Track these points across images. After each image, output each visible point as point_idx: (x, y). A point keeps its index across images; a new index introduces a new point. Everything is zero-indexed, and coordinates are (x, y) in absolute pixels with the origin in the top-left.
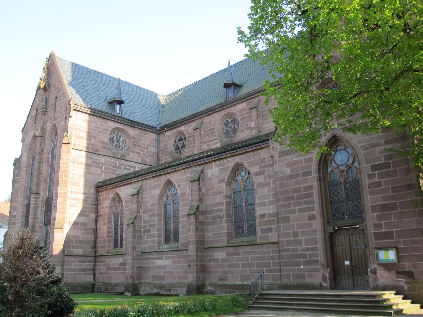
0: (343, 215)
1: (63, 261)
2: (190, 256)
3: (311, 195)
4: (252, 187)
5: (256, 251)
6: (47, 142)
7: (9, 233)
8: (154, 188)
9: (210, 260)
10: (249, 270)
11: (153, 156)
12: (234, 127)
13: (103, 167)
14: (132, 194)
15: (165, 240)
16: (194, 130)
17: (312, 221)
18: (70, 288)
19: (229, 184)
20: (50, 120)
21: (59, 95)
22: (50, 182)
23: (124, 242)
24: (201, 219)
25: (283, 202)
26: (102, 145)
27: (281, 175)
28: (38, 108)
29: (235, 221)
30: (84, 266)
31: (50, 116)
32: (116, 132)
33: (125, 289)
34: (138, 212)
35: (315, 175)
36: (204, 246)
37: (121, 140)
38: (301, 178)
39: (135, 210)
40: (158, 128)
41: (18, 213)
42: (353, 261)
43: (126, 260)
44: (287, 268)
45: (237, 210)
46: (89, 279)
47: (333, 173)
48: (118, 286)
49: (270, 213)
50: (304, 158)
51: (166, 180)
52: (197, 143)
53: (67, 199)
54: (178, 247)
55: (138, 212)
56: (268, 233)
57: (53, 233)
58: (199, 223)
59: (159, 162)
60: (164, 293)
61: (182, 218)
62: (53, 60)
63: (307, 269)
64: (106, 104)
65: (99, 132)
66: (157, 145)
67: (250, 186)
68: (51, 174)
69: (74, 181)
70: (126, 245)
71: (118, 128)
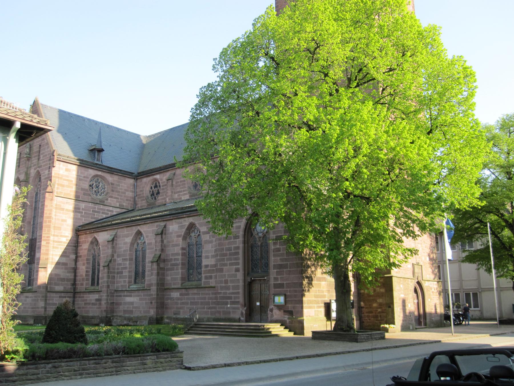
2: (152, 295)
5: (200, 292)
8: (127, 236)
9: (168, 299)
11: (130, 200)
16: (167, 180)
17: (237, 273)
19: (184, 238)
20: (33, 166)
21: (43, 144)
22: (34, 224)
23: (100, 281)
24: (162, 265)
25: (220, 257)
26: (83, 192)
28: (22, 153)
31: (34, 163)
32: (96, 179)
34: (113, 256)
35: (241, 239)
36: (163, 287)
37: (100, 186)
38: (232, 240)
40: (136, 174)
42: (262, 302)
44: (220, 306)
51: (136, 230)
52: (169, 192)
53: (50, 242)
54: (144, 287)
55: (113, 256)
57: (37, 271)
58: (160, 269)
59: (136, 205)
60: (132, 324)
62: (36, 108)
63: (232, 307)
64: (87, 152)
68: (34, 217)
70: (102, 284)
71: (97, 175)
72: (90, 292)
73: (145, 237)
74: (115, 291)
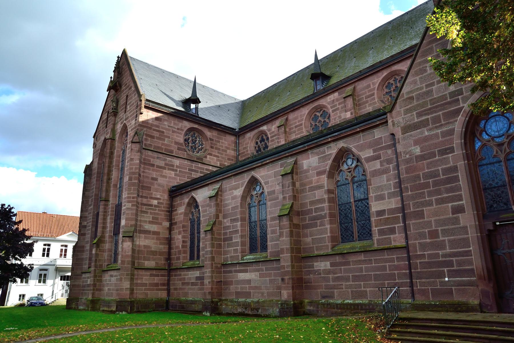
0: (506, 204)
1: (132, 275)
2: (283, 267)
3: (456, 179)
4: (363, 178)
6: (117, 144)
7: (79, 245)
8: (236, 188)
9: (309, 272)
10: (364, 284)
11: (232, 160)
12: (325, 121)
13: (177, 170)
14: (210, 196)
15: (250, 249)
18: (141, 306)
19: (331, 175)
21: (130, 93)
22: (120, 187)
23: (201, 253)
24: (295, 221)
26: (176, 146)
27: (408, 156)
29: (340, 222)
30: (156, 280)
32: (192, 133)
33: (203, 307)
34: (217, 216)
35: (459, 152)
37: (197, 141)
39: (213, 215)
41: (88, 223)
43: (203, 273)
45: (343, 208)
46: (163, 295)
47: (485, 149)
48: (195, 304)
49: (392, 208)
50: (440, 130)
51: (249, 177)
54: (267, 257)
55: (217, 216)
56: (390, 235)
60: (250, 313)
61: (271, 221)
63: (454, 281)
65: (173, 132)
66: (237, 148)
67: (359, 176)
69: (145, 185)
71: (193, 128)
72: (189, 268)
73: (263, 184)
74: (223, 265)
